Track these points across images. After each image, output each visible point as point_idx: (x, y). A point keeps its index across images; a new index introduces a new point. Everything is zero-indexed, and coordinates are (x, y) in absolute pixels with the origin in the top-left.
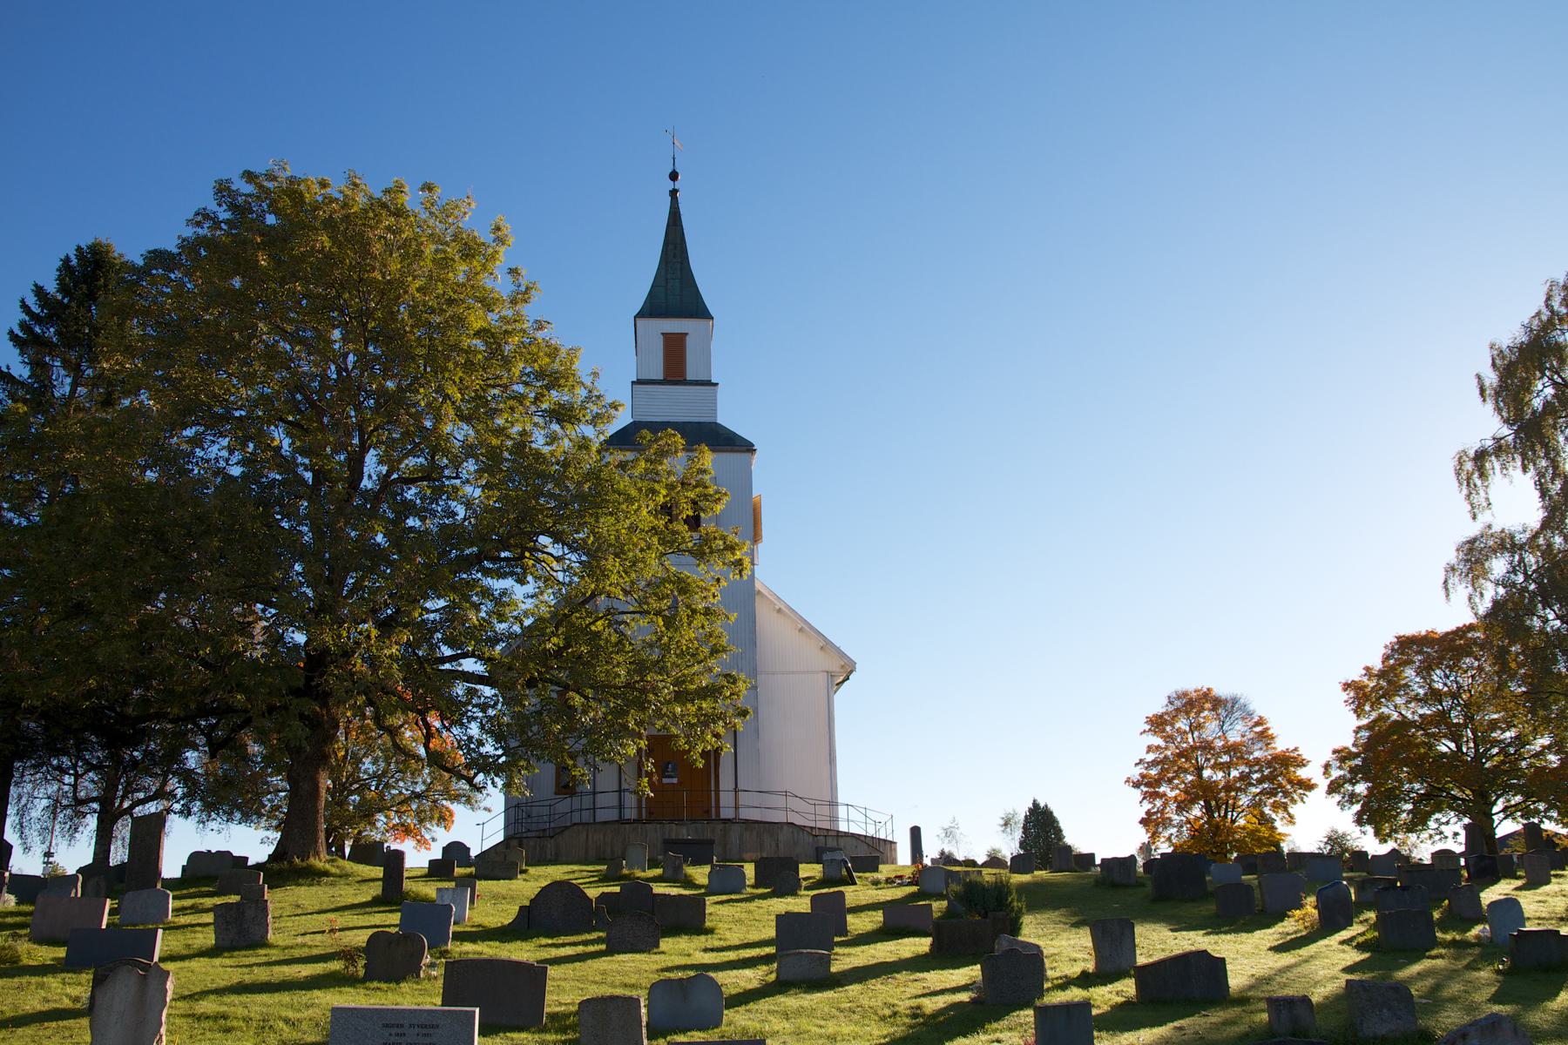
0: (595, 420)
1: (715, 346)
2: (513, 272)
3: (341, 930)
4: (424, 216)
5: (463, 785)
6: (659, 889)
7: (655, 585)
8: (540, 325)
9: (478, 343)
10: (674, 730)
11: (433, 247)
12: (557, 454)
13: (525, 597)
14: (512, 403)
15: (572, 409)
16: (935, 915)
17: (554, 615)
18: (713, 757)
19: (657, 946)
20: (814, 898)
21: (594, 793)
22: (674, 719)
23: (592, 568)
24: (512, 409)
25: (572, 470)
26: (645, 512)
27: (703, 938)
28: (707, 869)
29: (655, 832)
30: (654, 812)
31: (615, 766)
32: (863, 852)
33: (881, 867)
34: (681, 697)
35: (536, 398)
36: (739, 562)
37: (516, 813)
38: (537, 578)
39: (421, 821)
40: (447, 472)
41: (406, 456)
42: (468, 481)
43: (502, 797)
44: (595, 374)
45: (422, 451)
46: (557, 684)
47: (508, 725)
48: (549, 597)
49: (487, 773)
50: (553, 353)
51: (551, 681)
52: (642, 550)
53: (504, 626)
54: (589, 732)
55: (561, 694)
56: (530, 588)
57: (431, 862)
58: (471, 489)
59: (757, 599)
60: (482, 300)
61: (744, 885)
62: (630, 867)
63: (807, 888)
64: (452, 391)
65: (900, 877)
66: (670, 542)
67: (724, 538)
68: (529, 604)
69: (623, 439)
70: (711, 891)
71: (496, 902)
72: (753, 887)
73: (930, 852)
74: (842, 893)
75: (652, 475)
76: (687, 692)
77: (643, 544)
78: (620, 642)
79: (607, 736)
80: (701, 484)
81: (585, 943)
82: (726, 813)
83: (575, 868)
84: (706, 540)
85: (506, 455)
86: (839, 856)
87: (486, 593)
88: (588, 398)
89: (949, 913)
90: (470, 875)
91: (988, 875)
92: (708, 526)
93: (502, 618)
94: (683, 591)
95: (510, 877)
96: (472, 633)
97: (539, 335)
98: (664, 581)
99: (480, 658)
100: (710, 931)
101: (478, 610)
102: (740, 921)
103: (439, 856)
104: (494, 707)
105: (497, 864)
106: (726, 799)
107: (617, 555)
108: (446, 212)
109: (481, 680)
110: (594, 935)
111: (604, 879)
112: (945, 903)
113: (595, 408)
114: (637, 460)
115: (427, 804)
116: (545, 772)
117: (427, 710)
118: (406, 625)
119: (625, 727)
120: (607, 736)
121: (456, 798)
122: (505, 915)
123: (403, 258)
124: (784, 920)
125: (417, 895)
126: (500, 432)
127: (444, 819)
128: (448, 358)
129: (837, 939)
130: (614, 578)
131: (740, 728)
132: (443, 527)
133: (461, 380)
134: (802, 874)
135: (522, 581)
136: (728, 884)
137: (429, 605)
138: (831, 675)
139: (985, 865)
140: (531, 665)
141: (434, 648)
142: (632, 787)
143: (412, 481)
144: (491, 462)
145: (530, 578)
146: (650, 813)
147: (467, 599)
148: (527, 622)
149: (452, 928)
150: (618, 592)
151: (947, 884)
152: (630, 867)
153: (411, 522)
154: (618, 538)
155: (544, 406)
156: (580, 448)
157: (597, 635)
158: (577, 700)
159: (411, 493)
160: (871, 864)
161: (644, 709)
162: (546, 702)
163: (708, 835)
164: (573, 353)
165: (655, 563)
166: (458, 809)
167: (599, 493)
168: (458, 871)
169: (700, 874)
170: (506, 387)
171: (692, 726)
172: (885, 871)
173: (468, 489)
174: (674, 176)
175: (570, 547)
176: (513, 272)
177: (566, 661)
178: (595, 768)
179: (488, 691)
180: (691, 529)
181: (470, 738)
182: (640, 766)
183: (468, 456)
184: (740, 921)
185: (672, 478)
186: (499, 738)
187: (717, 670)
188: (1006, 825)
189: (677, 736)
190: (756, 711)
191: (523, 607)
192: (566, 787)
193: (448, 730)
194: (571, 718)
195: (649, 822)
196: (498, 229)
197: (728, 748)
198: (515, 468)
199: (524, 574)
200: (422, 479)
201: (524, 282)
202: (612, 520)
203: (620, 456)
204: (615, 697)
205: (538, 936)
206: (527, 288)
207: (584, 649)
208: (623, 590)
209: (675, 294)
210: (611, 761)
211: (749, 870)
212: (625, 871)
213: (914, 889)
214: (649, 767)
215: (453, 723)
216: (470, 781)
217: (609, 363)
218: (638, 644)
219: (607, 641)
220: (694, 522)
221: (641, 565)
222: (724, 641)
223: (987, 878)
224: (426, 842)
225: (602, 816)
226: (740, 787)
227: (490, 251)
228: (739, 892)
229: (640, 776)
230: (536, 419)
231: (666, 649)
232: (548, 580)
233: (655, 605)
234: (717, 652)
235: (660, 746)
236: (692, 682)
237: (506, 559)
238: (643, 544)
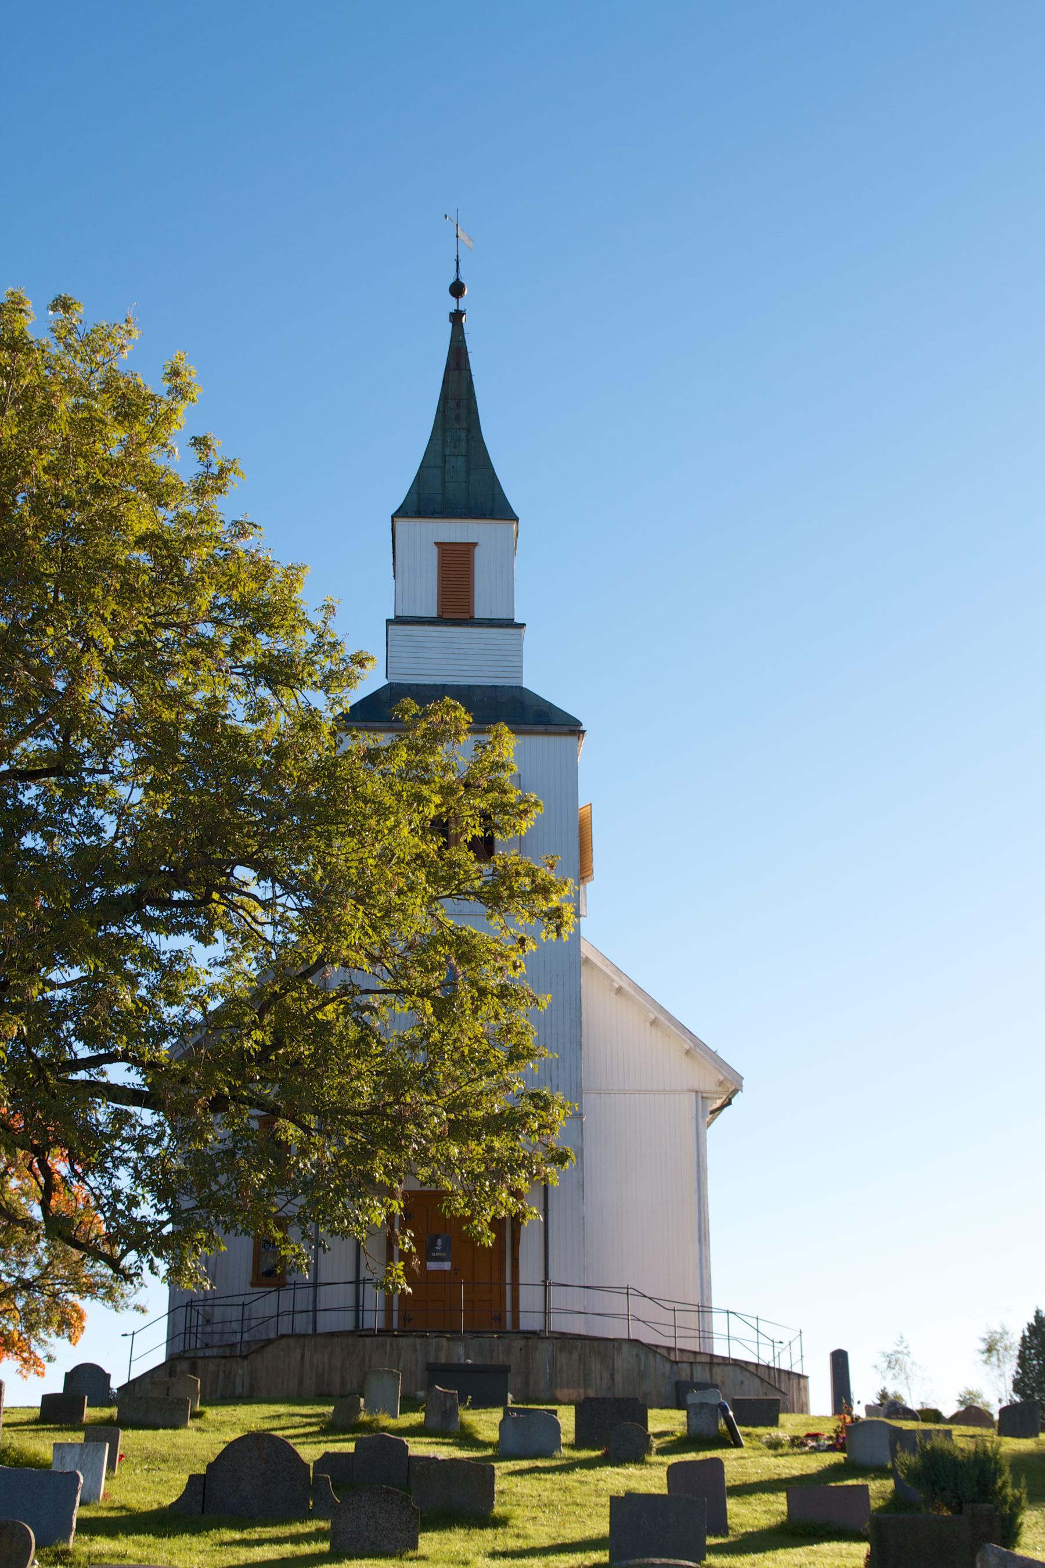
0: (326, 683)
1: (521, 565)
2: (200, 443)
4: (56, 350)
5: (103, 1269)
6: (419, 1448)
7: (421, 948)
8: (241, 529)
9: (142, 557)
10: (448, 1184)
11: (71, 401)
12: (267, 737)
13: (210, 964)
14: (195, 653)
15: (291, 663)
16: (875, 1504)
17: (257, 994)
18: (508, 1228)
19: (414, 1546)
20: (673, 1470)
21: (315, 1285)
22: (448, 1166)
23: (320, 918)
24: (195, 662)
25: (290, 763)
26: (405, 832)
27: (489, 1533)
28: (497, 1415)
29: (413, 1352)
30: (414, 1317)
31: (350, 1244)
32: (753, 1391)
33: (783, 1417)
34: (460, 1130)
35: (234, 646)
36: (556, 914)
37: (186, 1316)
38: (230, 934)
39: (31, 1328)
40: (88, 763)
41: (22, 736)
42: (122, 777)
43: (165, 1289)
44: (329, 609)
45: (49, 728)
46: (260, 1106)
47: (179, 1172)
48: (249, 965)
49: (142, 1251)
50: (262, 573)
51: (250, 1102)
52: (400, 893)
53: (175, 1010)
54: (310, 1185)
55: (267, 1123)
56: (219, 949)
57: (45, 1398)
58: (124, 796)
59: (584, 971)
60: (148, 488)
61: (557, 1444)
62: (371, 1408)
63: (661, 1452)
64: (100, 633)
65: (815, 1436)
66: (445, 878)
67: (532, 873)
68: (217, 976)
69: (373, 711)
70: (504, 1454)
71: (153, 1467)
72: (575, 1446)
73: (864, 1395)
74: (718, 1463)
75: (418, 773)
76: (470, 1122)
77: (402, 883)
78: (362, 1039)
79: (339, 1192)
80: (495, 786)
81: (296, 1539)
82: (530, 1322)
83: (281, 1409)
84: (503, 876)
85: (185, 736)
86: (714, 1398)
87: (149, 957)
88: (318, 648)
89: (897, 1502)
90: (109, 1422)
91: (963, 1439)
92: (506, 854)
93: (172, 997)
94: (465, 958)
95: (176, 1424)
96: (124, 1023)
97: (241, 545)
98: (434, 942)
99: (135, 1062)
100: (501, 1522)
101: (135, 985)
102: (549, 1505)
103: (59, 1389)
104: (156, 1142)
105: (154, 1402)
106: (530, 1298)
107: (359, 900)
108: (92, 345)
109: (135, 1097)
110: (311, 1526)
111: (330, 1429)
112: (889, 1484)
113: (327, 663)
114: (395, 747)
115: (41, 1299)
116: (236, 1250)
117: (48, 1146)
118: (16, 1009)
119: (368, 1177)
120: (339, 1192)
121: (88, 1289)
122: (163, 1490)
123: (23, 417)
124: (624, 1507)
125: (21, 1454)
126: (175, 699)
127: (69, 1324)
128: (93, 581)
129: (711, 1541)
130: (355, 936)
131: (554, 1182)
132: (80, 850)
133: (114, 614)
134: (653, 1427)
135: (205, 939)
136: (528, 1442)
137: (55, 976)
138: (703, 1097)
139: (956, 1419)
140: (219, 1075)
141: (60, 1044)
142: (379, 1276)
143: (29, 776)
144: (160, 750)
145: (218, 934)
146: (405, 1318)
147: (116, 965)
148: (213, 1005)
149: (78, 1512)
150: (359, 958)
151: (894, 1453)
152: (371, 1408)
153: (29, 841)
154: (361, 873)
155: (247, 659)
156: (304, 727)
157: (325, 1027)
158: (291, 1132)
159: (29, 795)
160: (765, 1412)
161: (397, 1148)
162: (240, 1135)
163: (500, 1358)
164: (293, 572)
165: (420, 913)
166: (91, 1307)
167: (333, 800)
168: (91, 1413)
169: (486, 1423)
170: (185, 627)
171: (477, 1177)
172: (789, 1425)
173: (122, 790)
174: (457, 289)
175: (285, 885)
176: (200, 443)
177: (275, 1069)
178: (319, 1245)
179: (147, 1116)
180: (479, 858)
181: (117, 1193)
182: (391, 1242)
183: (123, 737)
184: (550, 1505)
185: (451, 777)
186: (163, 1193)
187: (518, 1087)
188: (990, 1350)
189: (452, 1193)
190: (580, 1153)
191: (208, 980)
192: (269, 1274)
193: (81, 1179)
194: (281, 1162)
195: (404, 1333)
196: (176, 373)
197: (534, 1214)
198: (199, 757)
199: (210, 927)
200: (48, 773)
201: (217, 461)
202: (353, 843)
203: (367, 740)
204: (354, 1128)
205: (218, 1526)
206: (222, 470)
207: (305, 1050)
208: (369, 956)
209: (457, 480)
210: (345, 1233)
211: (566, 1418)
212: (363, 1417)
213: (838, 1457)
214: (406, 1243)
215: (89, 1168)
216: (114, 1263)
217: (351, 589)
218: (391, 1040)
219: (342, 1037)
220: (484, 848)
221: (397, 916)
222: (530, 1041)
223: (962, 1443)
224: (37, 1362)
225: (328, 1323)
226: (553, 1278)
227: (163, 408)
228: (548, 1455)
229: (390, 1258)
230: (234, 679)
231: (436, 1051)
232: (249, 937)
233: (418, 979)
234: (519, 1057)
235: (424, 1209)
236: (477, 1106)
237: (180, 903)
238: (402, 883)
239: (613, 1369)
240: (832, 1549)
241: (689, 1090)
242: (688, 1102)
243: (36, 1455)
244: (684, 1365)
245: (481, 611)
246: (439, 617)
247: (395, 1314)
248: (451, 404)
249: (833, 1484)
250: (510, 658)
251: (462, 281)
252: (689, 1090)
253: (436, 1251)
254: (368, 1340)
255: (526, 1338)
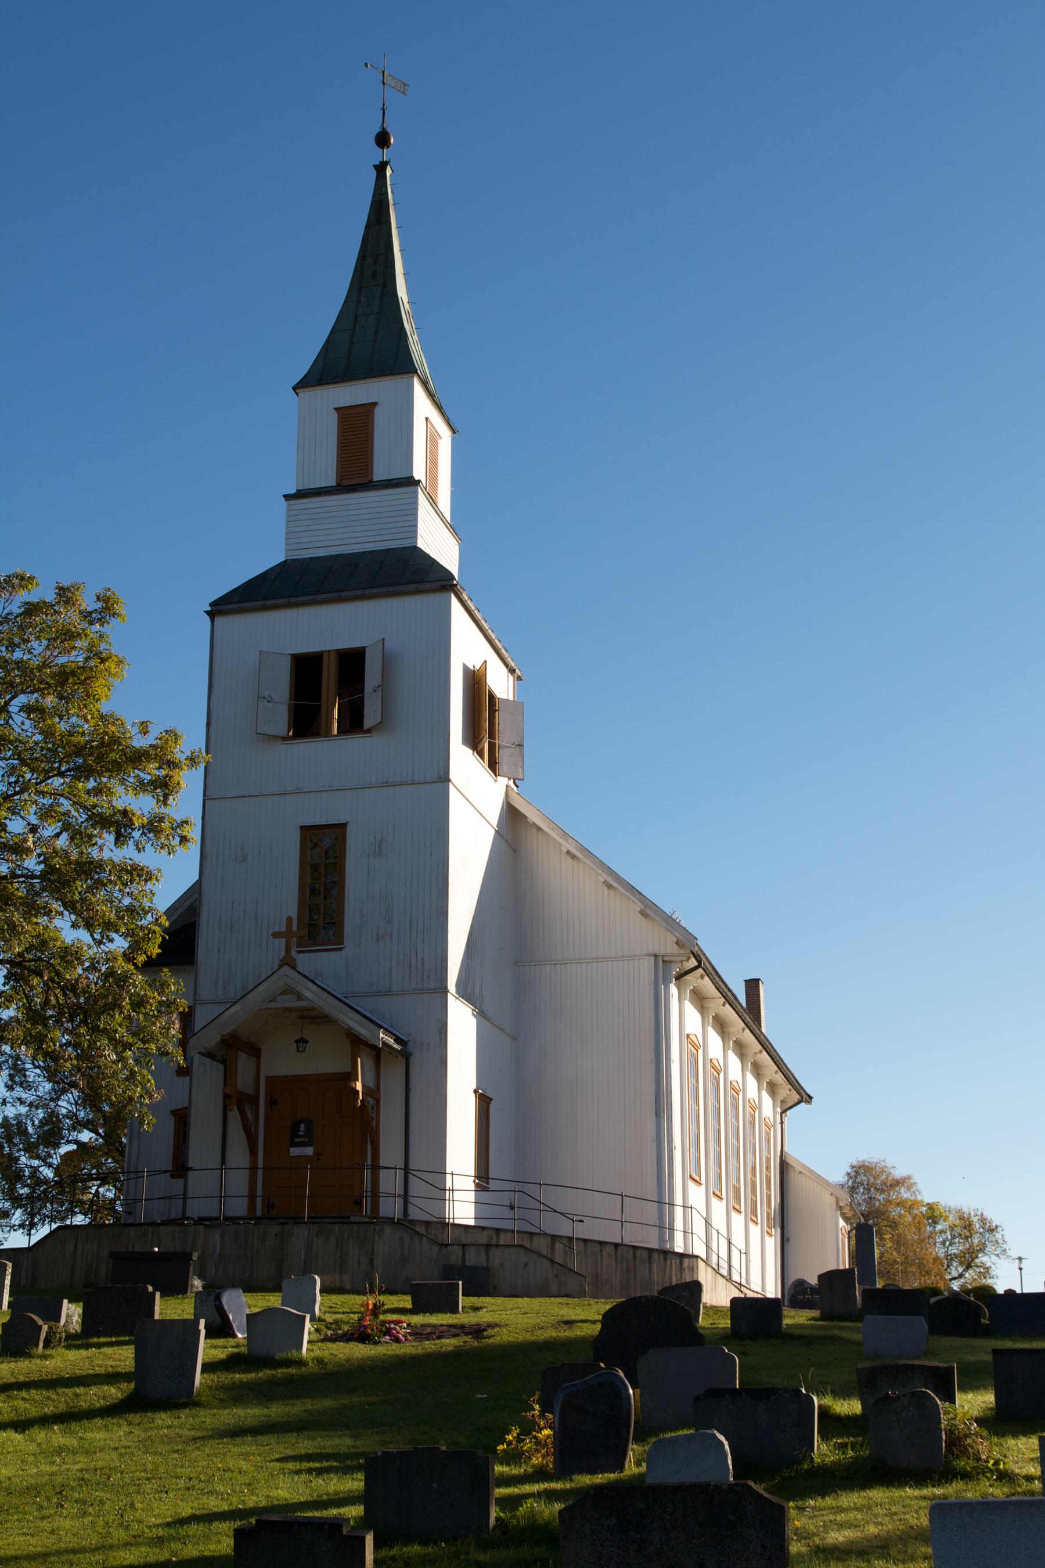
3: (386, 784)
106: (390, 1182)
146: (269, 1206)
174: (382, 140)
239: (373, 1251)
240: (25, 1409)
241: (647, 955)
242: (646, 967)
243: (348, 1360)
244: (456, 1248)
245: (379, 474)
246: (338, 485)
247: (259, 1200)
248: (369, 261)
249: (621, 1374)
250: (405, 518)
251: (389, 130)
252: (647, 955)
253: (299, 1136)
254: (132, 1230)
255: (282, 1223)
